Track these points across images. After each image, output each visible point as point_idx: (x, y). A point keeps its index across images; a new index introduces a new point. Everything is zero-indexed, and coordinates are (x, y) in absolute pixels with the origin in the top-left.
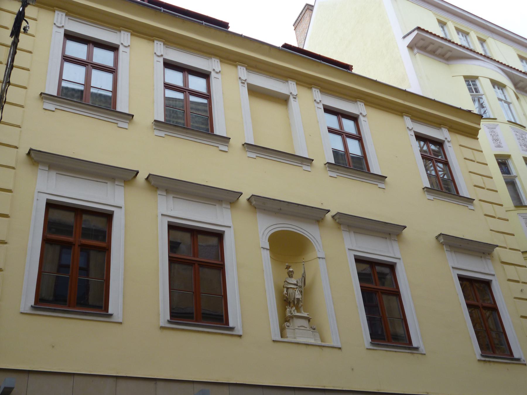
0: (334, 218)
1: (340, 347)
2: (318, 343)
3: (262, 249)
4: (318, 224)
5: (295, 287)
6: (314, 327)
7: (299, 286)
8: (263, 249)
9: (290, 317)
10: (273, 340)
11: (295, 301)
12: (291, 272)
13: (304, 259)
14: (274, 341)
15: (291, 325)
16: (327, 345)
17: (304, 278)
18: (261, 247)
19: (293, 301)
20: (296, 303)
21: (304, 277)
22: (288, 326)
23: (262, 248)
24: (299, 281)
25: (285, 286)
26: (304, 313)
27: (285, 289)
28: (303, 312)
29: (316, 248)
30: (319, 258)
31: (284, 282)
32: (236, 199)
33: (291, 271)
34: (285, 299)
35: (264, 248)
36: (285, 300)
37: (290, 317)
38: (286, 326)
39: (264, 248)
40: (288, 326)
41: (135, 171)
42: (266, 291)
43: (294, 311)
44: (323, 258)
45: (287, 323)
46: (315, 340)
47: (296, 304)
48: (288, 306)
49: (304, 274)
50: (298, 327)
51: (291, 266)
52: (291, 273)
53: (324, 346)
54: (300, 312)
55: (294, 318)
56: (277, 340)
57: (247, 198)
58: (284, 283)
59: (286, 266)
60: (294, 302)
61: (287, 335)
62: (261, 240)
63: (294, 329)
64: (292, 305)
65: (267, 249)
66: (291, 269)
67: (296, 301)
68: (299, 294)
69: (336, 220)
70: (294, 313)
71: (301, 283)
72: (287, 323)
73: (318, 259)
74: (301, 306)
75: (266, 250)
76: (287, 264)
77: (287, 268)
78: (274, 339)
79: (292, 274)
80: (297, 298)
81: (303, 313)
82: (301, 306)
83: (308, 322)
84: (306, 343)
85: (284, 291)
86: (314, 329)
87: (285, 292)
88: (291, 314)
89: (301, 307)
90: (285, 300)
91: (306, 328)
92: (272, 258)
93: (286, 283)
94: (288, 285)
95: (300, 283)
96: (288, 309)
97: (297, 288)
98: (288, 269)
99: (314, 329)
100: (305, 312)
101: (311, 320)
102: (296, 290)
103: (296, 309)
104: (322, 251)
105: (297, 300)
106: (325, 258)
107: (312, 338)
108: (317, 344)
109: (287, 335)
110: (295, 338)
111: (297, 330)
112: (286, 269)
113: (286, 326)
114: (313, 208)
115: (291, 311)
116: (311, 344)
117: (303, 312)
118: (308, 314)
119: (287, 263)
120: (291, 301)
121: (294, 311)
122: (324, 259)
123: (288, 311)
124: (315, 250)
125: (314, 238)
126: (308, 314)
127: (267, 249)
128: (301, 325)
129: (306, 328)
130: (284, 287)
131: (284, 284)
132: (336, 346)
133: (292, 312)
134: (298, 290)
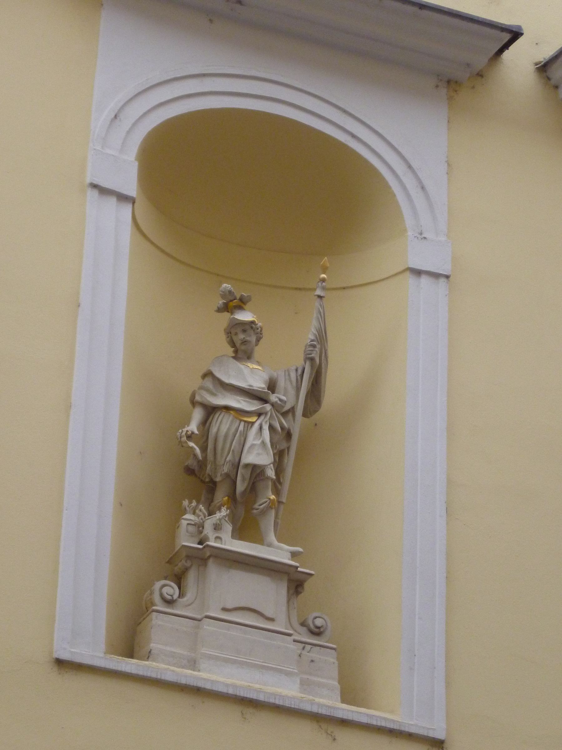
0: (549, 79)
1: (440, 735)
2: (312, 703)
3: (93, 194)
4: (450, 99)
5: (251, 406)
6: (319, 622)
7: (273, 405)
8: (95, 193)
9: (188, 557)
10: (56, 655)
11: (239, 478)
12: (244, 331)
13: (324, 270)
14: (60, 663)
15: (190, 595)
16: (364, 720)
17: (312, 366)
18: (88, 180)
19: (227, 475)
20: (240, 487)
21: (312, 360)
22: (170, 602)
23: (94, 186)
24: (281, 383)
25: (198, 398)
26: (276, 543)
27: (198, 415)
28: (272, 537)
29: (409, 221)
30: (418, 273)
31: (205, 376)
32: (485, 60)
33: (242, 324)
34: (190, 462)
35: (103, 191)
36: (189, 471)
37: (188, 557)
38: (157, 598)
39: (103, 191)
40: (170, 602)
41: (503, 29)
42: (69, 407)
43: (217, 527)
44: (436, 276)
45: (164, 586)
46: (305, 685)
47: (244, 493)
48: (190, 502)
49: (314, 346)
50: (225, 610)
51: (249, 299)
52: (242, 336)
53: (344, 723)
54: (258, 539)
55: (211, 562)
56: (78, 659)
57: (537, 60)
58: (199, 381)
59: (223, 296)
60: (234, 483)
61: (152, 645)
62: (99, 148)
63: (200, 620)
64: (221, 496)
65: (122, 198)
66: (245, 316)
67: (244, 479)
68: (263, 443)
69: (556, 87)
70: (218, 538)
71: (292, 392)
72: (164, 586)
73: (411, 279)
74: (269, 508)
75: (113, 200)
76: (226, 286)
77: (226, 308)
78: (65, 656)
79: (244, 342)
80: (247, 466)
81: (270, 545)
82: (269, 508)
83: (283, 591)
84: (242, 694)
85: (188, 422)
86: (317, 632)
87: (193, 427)
88: (200, 543)
89: (264, 513)
90: (189, 471)
91: (272, 620)
92: (162, 251)
93: (208, 383)
94: (213, 394)
95: (285, 389)
96: (187, 516)
97: (259, 415)
98: (232, 313)
99: (317, 632)
100: (279, 541)
101: (307, 585)
102: (253, 423)
103: (233, 518)
104: (443, 238)
105: (248, 476)
106: (447, 277)
107: (288, 674)
108: (307, 707)
109: (152, 645)
110: (193, 664)
111: (209, 627)
112: (219, 310)
113: (157, 598)
114: (425, 13)
115: (200, 527)
116: (272, 700)
117: (272, 537)
118: (294, 555)
119: (228, 279)
120: (218, 479)
121: (217, 527)
122: (442, 280)
123: (184, 523)
124: (405, 230)
125: (410, 167)
126: (294, 555)
127: (122, 198)
128: (242, 605)
129: (272, 620)
130: (194, 403)
131: (202, 388)
132: (413, 730)
133: (208, 530)
134: (266, 427)
